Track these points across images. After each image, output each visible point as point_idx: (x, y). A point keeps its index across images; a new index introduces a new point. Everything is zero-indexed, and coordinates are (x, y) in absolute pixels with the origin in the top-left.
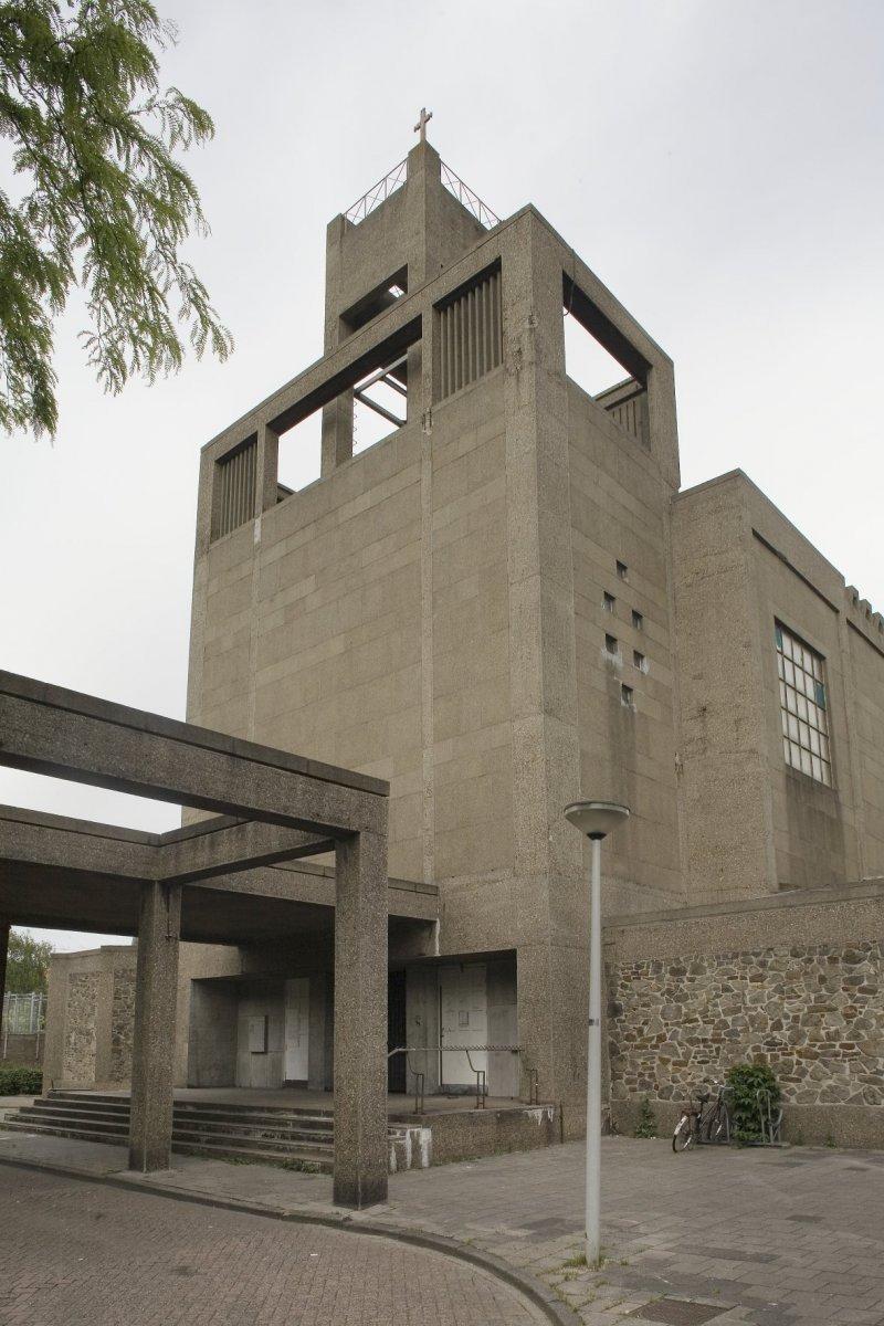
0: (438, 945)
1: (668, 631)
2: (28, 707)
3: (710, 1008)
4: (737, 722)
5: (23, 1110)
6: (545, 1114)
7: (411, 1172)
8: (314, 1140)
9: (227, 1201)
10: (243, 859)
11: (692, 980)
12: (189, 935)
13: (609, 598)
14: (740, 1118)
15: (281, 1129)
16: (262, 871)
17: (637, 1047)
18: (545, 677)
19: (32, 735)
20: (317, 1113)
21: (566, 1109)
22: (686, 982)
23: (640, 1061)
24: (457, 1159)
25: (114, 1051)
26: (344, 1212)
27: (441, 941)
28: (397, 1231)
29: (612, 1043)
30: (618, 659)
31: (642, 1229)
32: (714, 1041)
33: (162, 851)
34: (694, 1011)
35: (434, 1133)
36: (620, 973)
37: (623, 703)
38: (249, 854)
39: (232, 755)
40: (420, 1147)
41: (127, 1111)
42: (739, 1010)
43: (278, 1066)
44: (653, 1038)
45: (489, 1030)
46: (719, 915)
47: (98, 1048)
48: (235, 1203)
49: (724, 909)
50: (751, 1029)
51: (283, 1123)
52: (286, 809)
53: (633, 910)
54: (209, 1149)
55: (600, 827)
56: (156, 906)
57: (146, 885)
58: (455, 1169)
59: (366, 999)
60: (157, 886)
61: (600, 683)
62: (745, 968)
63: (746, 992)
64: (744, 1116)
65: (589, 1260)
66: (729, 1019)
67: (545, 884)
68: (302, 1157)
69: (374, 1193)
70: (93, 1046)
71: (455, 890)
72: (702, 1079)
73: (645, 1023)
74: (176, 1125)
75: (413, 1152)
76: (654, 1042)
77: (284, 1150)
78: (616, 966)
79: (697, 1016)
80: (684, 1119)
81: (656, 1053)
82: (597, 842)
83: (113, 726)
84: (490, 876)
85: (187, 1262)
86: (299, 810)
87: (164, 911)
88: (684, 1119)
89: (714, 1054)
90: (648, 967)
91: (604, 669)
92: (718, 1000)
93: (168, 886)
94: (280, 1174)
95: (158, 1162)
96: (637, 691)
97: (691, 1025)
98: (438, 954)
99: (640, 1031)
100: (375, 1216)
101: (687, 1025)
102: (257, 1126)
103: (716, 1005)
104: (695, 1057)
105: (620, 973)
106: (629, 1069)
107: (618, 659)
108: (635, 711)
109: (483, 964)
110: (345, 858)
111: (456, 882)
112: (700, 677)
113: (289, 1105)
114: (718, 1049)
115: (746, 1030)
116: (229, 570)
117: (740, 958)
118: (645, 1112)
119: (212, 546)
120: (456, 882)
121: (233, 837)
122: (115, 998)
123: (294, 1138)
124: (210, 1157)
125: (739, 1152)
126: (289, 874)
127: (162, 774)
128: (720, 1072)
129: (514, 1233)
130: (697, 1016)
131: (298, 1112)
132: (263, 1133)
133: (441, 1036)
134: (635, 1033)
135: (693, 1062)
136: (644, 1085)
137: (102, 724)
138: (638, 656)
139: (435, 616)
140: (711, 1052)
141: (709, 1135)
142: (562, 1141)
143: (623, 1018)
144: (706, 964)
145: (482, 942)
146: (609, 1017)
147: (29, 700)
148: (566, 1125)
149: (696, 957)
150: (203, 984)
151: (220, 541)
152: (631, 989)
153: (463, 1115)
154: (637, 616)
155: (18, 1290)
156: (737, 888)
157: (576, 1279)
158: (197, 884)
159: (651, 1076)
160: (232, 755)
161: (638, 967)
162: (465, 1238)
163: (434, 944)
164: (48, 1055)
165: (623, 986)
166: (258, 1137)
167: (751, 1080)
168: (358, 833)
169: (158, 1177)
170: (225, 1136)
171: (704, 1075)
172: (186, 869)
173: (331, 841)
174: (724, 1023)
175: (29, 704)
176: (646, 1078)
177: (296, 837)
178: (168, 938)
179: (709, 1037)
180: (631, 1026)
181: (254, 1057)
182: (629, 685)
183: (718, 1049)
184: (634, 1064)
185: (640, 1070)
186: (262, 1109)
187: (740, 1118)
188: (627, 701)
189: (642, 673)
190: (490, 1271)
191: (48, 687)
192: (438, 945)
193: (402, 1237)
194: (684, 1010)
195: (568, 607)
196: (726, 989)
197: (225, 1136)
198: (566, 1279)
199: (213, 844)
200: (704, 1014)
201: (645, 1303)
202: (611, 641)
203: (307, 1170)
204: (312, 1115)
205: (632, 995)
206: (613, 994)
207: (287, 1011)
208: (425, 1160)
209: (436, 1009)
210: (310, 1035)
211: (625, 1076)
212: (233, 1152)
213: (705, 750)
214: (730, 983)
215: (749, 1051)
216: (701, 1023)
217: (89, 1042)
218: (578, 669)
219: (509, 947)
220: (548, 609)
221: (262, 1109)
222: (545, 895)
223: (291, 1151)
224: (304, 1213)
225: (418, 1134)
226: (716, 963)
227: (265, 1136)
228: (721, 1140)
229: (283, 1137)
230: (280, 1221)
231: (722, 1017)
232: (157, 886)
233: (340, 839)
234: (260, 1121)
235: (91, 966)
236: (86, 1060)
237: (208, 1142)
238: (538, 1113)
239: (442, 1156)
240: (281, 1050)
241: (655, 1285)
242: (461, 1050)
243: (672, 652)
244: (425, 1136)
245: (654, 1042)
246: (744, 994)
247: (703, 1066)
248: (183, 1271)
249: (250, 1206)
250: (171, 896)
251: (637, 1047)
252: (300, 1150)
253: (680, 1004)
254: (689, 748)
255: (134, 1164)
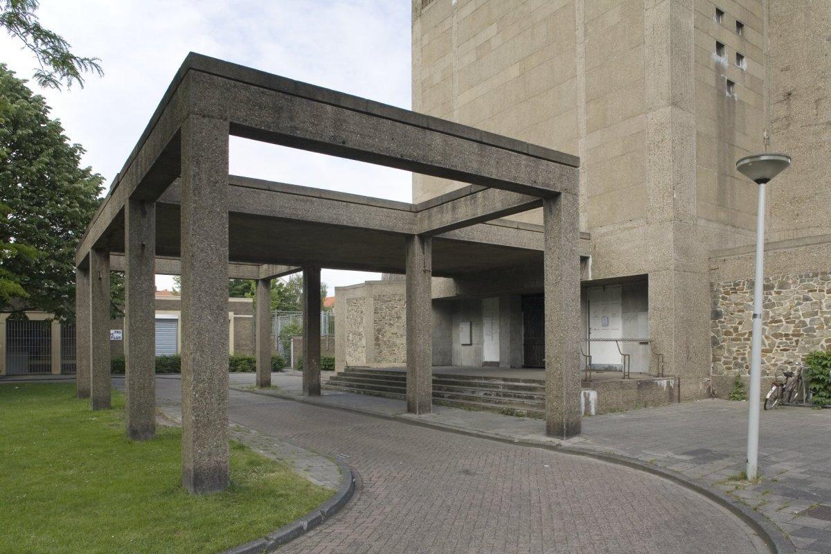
0: (590, 272)
1: (763, 35)
2: (357, 116)
3: (793, 312)
4: (817, 102)
5: (331, 378)
6: (668, 383)
7: (584, 418)
8: (519, 397)
9: (475, 432)
10: (477, 216)
11: (778, 293)
12: (436, 273)
13: (720, 13)
14: (815, 388)
15: (496, 390)
16: (480, 226)
17: (733, 340)
18: (672, 77)
19: (361, 135)
20: (517, 380)
21: (682, 380)
22: (774, 295)
23: (735, 349)
24: (613, 411)
25: (376, 345)
26: (556, 441)
27: (593, 270)
28: (597, 453)
29: (714, 337)
30: (724, 60)
31: (773, 459)
32: (793, 335)
33: (419, 215)
34: (779, 315)
35: (599, 394)
36: (721, 289)
37: (727, 93)
38: (480, 213)
39: (481, 142)
40: (590, 402)
41: (405, 379)
42: (816, 313)
43: (479, 353)
44: (745, 334)
45: (624, 328)
46: (803, 246)
47: (367, 343)
48: (480, 433)
49: (808, 241)
50: (825, 327)
51: (496, 386)
52: (515, 178)
53: (730, 245)
54: (451, 402)
55: (766, 174)
56: (416, 251)
57: (409, 237)
58: (614, 416)
59: (567, 305)
60: (416, 237)
61: (711, 79)
62: (823, 284)
63: (823, 301)
64: (818, 387)
65: (749, 477)
66: (808, 320)
67: (671, 228)
68: (513, 407)
69: (573, 430)
70: (364, 342)
71: (603, 235)
72: (783, 362)
73: (740, 323)
74: (434, 388)
75: (585, 406)
76: (746, 336)
77: (500, 403)
78: (719, 284)
79: (782, 318)
80: (774, 388)
81: (747, 344)
82: (763, 185)
83: (408, 126)
84: (629, 225)
85: (467, 467)
86: (523, 180)
87: (421, 254)
88: (774, 388)
89: (794, 344)
90: (744, 285)
91: (713, 68)
92: (799, 307)
93: (423, 237)
94: (501, 417)
95: (424, 409)
96: (738, 84)
97: (776, 325)
98: (590, 279)
99: (736, 329)
100: (575, 444)
101: (773, 324)
102: (481, 388)
103: (797, 310)
104: (778, 347)
105: (721, 289)
106: (726, 354)
107: (724, 60)
108: (736, 99)
109: (618, 285)
110: (551, 212)
111: (604, 230)
112: (787, 69)
113: (496, 376)
114: (797, 342)
115: (821, 328)
116: (436, 26)
117: (820, 276)
118: (737, 383)
119: (423, 11)
120: (604, 230)
121: (468, 202)
122: (375, 313)
123: (505, 395)
124: (452, 406)
125: (818, 411)
126: (495, 228)
127: (439, 158)
128: (798, 356)
129: (677, 457)
130: (782, 318)
131: (505, 380)
132: (484, 392)
133: (589, 333)
134: (732, 330)
135: (777, 350)
136: (737, 365)
137: (402, 125)
138: (740, 57)
139: (587, 41)
140: (793, 343)
141: (789, 398)
142: (679, 401)
143: (723, 320)
144: (790, 281)
145: (622, 269)
146: (712, 319)
147: (358, 111)
148: (682, 390)
149: (783, 277)
150: (438, 304)
151: (428, 7)
152: (730, 300)
153: (617, 382)
154: (740, 25)
155: (373, 479)
156: (809, 227)
157: (744, 489)
158: (440, 236)
159: (743, 359)
160: (481, 142)
161: (736, 285)
162: (649, 459)
163: (588, 272)
164: (337, 347)
165: (723, 298)
166: (481, 394)
167: (824, 362)
168: (559, 194)
169: (426, 417)
170: (460, 394)
171: (785, 358)
172: (436, 226)
173: (540, 200)
174: (804, 324)
175: (358, 114)
176: (739, 361)
177: (514, 198)
178: (425, 271)
179: (791, 332)
180: (729, 326)
181: (463, 347)
182: (732, 80)
183: (797, 342)
184: (729, 351)
185: (735, 355)
186: (480, 378)
187: (815, 388)
188: (729, 91)
189: (742, 70)
190: (673, 480)
191: (368, 102)
192: (590, 272)
193: (600, 457)
194: (771, 314)
195: (690, 22)
196: (807, 299)
197: (460, 394)
198: (737, 488)
199: (454, 208)
200: (787, 317)
201: (807, 507)
202: (720, 46)
203: (517, 415)
204: (514, 382)
205: (731, 304)
206: (715, 304)
207: (485, 321)
208: (593, 411)
209: (586, 317)
210: (500, 333)
211: (723, 359)
212: (468, 404)
213: (789, 125)
214: (810, 295)
215: (823, 342)
216: (784, 323)
217: (360, 339)
218: (696, 70)
219: (643, 273)
220: (675, 26)
221: (480, 378)
222: (670, 236)
223: (504, 403)
224: (529, 440)
225: (589, 394)
226: (799, 281)
227: (486, 394)
228: (799, 402)
229: (498, 395)
230: (512, 445)
231: (802, 319)
232: (416, 237)
233: (545, 198)
234: (480, 385)
235: (359, 293)
236: (360, 350)
237: (449, 397)
238: (664, 383)
239: (605, 408)
240: (481, 342)
241: (807, 496)
242: (613, 340)
243: (765, 51)
244: (593, 395)
245: (746, 336)
246: (821, 303)
247: (785, 352)
248: (467, 472)
249: (490, 435)
250: (425, 247)
251: (733, 340)
252: (511, 403)
253: (768, 310)
254: (775, 125)
255: (411, 409)
